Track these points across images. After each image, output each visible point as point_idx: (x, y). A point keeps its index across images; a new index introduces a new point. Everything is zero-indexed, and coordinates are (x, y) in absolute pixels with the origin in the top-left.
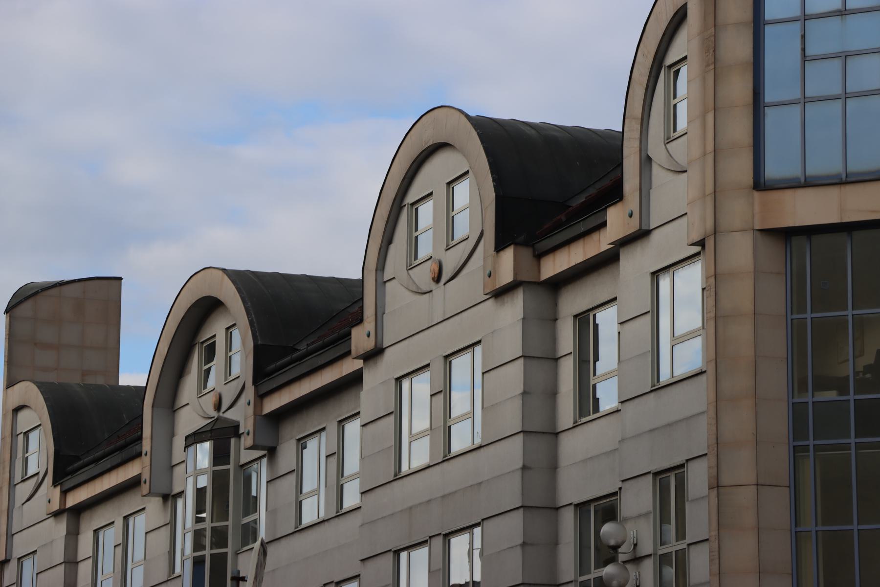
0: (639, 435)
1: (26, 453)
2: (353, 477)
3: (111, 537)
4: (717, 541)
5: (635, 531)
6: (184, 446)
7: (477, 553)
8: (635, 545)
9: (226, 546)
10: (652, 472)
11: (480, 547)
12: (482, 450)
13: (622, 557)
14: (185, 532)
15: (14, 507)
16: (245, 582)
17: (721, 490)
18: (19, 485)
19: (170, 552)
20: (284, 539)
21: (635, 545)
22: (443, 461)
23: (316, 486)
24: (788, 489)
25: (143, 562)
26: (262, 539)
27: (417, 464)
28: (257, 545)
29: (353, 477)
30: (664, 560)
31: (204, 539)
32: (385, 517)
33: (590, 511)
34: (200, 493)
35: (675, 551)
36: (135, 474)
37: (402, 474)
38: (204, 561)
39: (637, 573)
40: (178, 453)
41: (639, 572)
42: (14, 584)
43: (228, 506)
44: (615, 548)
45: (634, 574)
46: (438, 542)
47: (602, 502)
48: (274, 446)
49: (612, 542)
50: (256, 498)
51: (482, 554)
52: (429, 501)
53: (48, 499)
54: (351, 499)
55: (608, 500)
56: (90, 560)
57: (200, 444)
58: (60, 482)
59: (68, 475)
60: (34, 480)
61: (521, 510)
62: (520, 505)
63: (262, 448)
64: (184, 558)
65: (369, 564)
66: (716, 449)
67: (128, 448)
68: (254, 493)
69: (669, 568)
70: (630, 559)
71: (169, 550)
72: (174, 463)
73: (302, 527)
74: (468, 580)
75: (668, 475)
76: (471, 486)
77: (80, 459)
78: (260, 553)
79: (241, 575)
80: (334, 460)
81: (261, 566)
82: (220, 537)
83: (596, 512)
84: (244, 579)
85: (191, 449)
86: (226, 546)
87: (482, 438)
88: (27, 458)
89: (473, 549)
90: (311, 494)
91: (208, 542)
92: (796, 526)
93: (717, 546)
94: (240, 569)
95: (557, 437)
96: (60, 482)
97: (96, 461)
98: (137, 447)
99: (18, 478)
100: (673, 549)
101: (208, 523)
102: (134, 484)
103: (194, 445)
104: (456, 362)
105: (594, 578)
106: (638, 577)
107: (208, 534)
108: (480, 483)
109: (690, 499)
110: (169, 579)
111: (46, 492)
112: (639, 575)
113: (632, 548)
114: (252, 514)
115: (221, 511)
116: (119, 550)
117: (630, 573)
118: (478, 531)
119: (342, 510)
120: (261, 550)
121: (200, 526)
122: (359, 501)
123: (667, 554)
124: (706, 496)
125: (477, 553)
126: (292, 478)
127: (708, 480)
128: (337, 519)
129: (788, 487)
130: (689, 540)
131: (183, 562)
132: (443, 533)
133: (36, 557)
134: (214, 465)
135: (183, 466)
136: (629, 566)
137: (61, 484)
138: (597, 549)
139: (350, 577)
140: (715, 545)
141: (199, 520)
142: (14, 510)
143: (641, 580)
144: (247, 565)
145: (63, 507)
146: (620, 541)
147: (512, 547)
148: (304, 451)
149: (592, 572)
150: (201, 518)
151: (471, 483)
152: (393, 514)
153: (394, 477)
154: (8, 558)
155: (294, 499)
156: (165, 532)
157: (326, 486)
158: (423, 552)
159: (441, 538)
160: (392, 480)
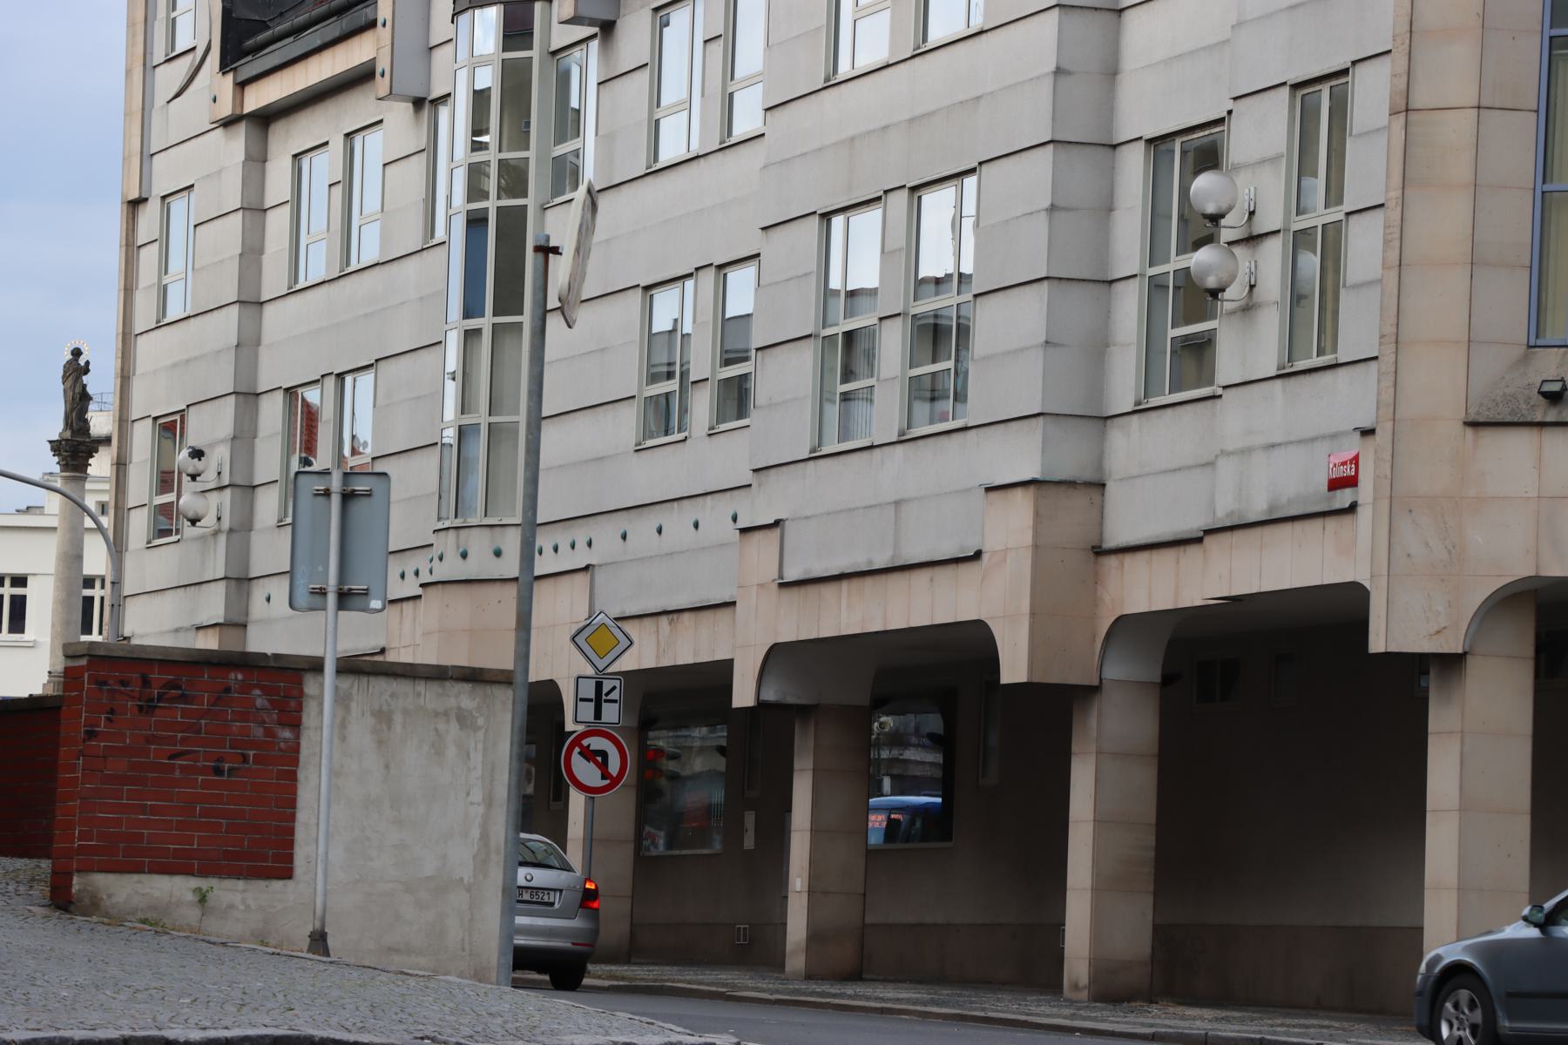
0: (1268, 16)
1: (173, 11)
2: (751, 81)
3: (323, 168)
4: (1399, 208)
5: (1252, 189)
6: (451, 12)
7: (968, 224)
8: (1252, 213)
9: (525, 195)
10: (1289, 83)
11: (974, 213)
12: (984, 36)
13: (1226, 235)
14: (453, 165)
15: (153, 107)
16: (559, 256)
17: (1413, 117)
18: (162, 67)
19: (425, 200)
20: (627, 185)
21: (1252, 213)
22: (913, 57)
23: (685, 95)
24: (1535, 114)
25: (379, 216)
26: (590, 182)
27: (865, 61)
28: (580, 194)
29: (751, 81)
30: (1301, 239)
31: (486, 179)
32: (805, 154)
33: (1173, 151)
34: (480, 98)
35: (1323, 225)
36: (365, 59)
37: (840, 78)
38: (486, 220)
39: (1253, 263)
40: (441, 26)
41: (1256, 262)
42: (156, 240)
43: (528, 124)
44: (1215, 219)
45: (1247, 264)
46: (899, 201)
47: (1195, 136)
48: (613, 19)
49: (1211, 209)
50: (578, 111)
51: (977, 225)
52: (885, 128)
53: (213, 97)
54: (744, 125)
55: (1207, 133)
56: (287, 208)
57: (480, 10)
58: (233, 66)
59: (247, 54)
60: (188, 59)
61: (1050, 147)
62: (1049, 139)
63: (592, 22)
64: (450, 212)
65: (777, 234)
66: (1407, 41)
67: (352, 11)
68: (574, 103)
69: (1310, 255)
70: (1241, 238)
71: (424, 197)
72: (433, 42)
73: (659, 166)
74: (950, 271)
75: (1318, 88)
76: (962, 102)
77: (268, 28)
78: (586, 208)
79: (552, 244)
80: (717, 48)
81: (586, 230)
82: (514, 177)
83: (1184, 153)
84: (556, 251)
85: (464, 19)
86: (525, 195)
87: (986, 16)
88: (174, 20)
89: (961, 217)
90: (675, 109)
91: (492, 185)
92: (1544, 182)
93: (1399, 217)
94: (548, 233)
95: (1120, 16)
96: (233, 66)
97: (297, 31)
98: (368, 10)
99: (159, 55)
100: (1319, 222)
101: (493, 152)
102: (362, 76)
103: (470, 11)
104: (930, 199)
105: (1174, 271)
106: (1253, 270)
107: (493, 171)
108: (978, 98)
109: (1354, 132)
110: (424, 247)
111: (209, 82)
112: (1256, 266)
113: (1246, 218)
114: (571, 139)
115: (518, 132)
116: (338, 192)
117: (1240, 263)
118: (970, 182)
119: (731, 139)
120: (587, 202)
121: (479, 157)
122: (760, 123)
123: (1308, 231)
124: (1384, 128)
125: (968, 224)
126: (643, 77)
127: (1391, 98)
128: (720, 154)
129: (1535, 111)
130: (1348, 207)
131: (449, 219)
132: (908, 185)
133: (193, 195)
134: (504, 50)
135: (449, 48)
136: (1238, 250)
137: (235, 69)
138: (1181, 217)
139: (742, 257)
140: (1396, 215)
141: (477, 147)
142: (153, 111)
143: (1258, 275)
144: (561, 226)
145: (238, 112)
146: (1224, 206)
147: (1032, 213)
148: (665, 30)
149: (1172, 260)
150: (481, 142)
151: (961, 97)
152: (820, 149)
153: (825, 82)
154: (144, 196)
155: (646, 115)
156: (419, 163)
157: (703, 95)
158: (873, 216)
159: (905, 193)
160: (820, 87)
